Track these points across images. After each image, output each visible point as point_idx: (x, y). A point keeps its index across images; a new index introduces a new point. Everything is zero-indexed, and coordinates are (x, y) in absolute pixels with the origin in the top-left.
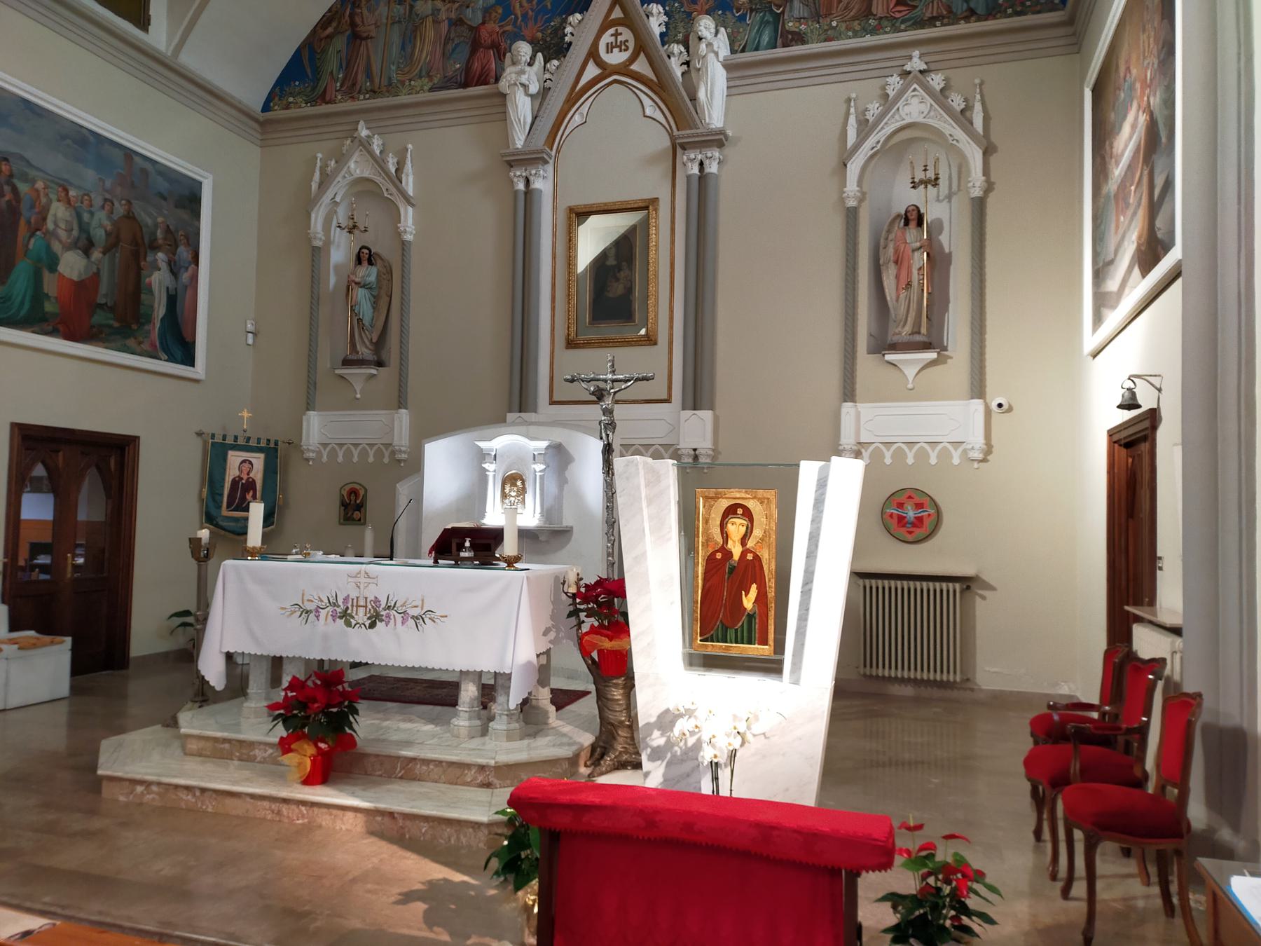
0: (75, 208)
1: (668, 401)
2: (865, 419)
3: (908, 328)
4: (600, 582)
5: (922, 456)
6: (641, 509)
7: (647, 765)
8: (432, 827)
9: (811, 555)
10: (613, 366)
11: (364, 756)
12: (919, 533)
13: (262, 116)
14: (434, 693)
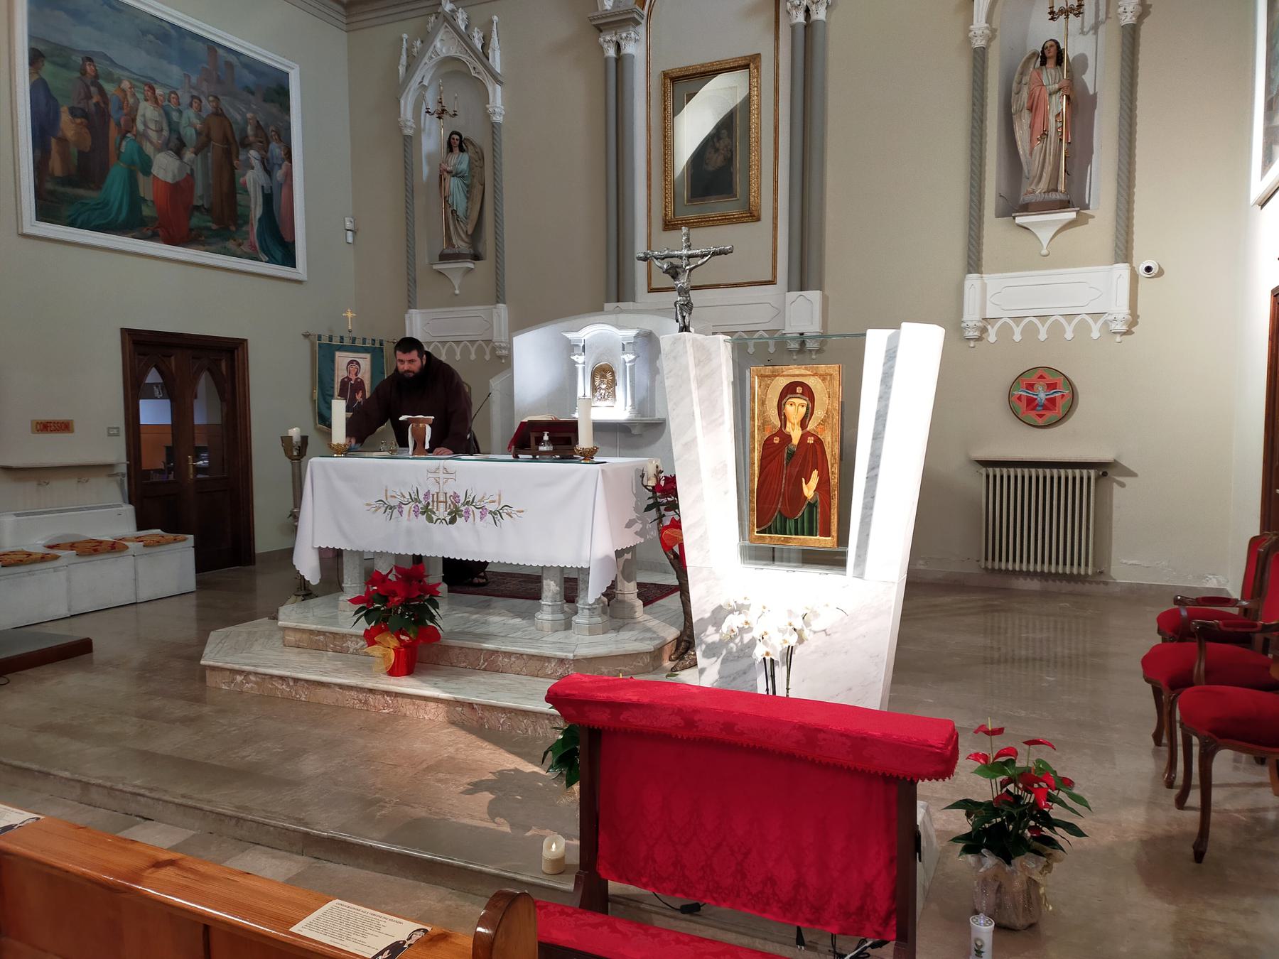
0: (163, 107)
1: (772, 282)
3: (1043, 185)
5: (1056, 330)
6: (690, 392)
7: (702, 662)
9: (878, 437)
10: (688, 240)
11: (449, 648)
12: (1050, 416)
14: (521, 586)
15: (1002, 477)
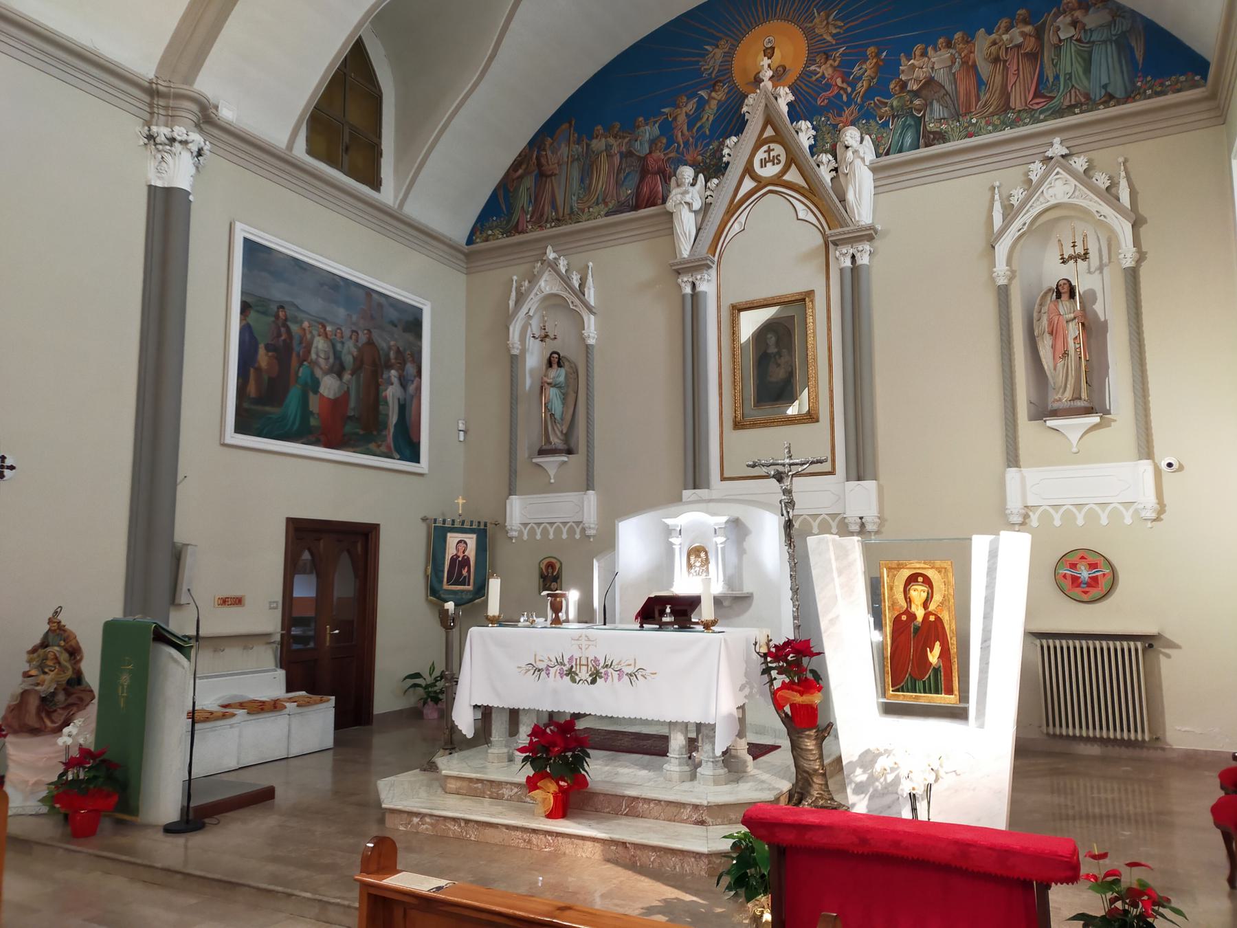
1: (832, 473)
2: (1031, 485)
3: (1068, 394)
4: (788, 643)
5: (1092, 517)
6: (833, 580)
8: (659, 857)
9: (988, 616)
11: (595, 794)
12: (1095, 593)
13: (466, 249)
14: (647, 744)
15: (1102, 649)
